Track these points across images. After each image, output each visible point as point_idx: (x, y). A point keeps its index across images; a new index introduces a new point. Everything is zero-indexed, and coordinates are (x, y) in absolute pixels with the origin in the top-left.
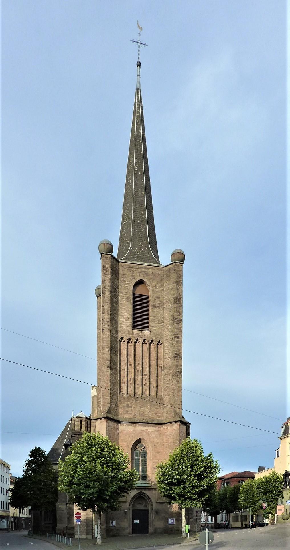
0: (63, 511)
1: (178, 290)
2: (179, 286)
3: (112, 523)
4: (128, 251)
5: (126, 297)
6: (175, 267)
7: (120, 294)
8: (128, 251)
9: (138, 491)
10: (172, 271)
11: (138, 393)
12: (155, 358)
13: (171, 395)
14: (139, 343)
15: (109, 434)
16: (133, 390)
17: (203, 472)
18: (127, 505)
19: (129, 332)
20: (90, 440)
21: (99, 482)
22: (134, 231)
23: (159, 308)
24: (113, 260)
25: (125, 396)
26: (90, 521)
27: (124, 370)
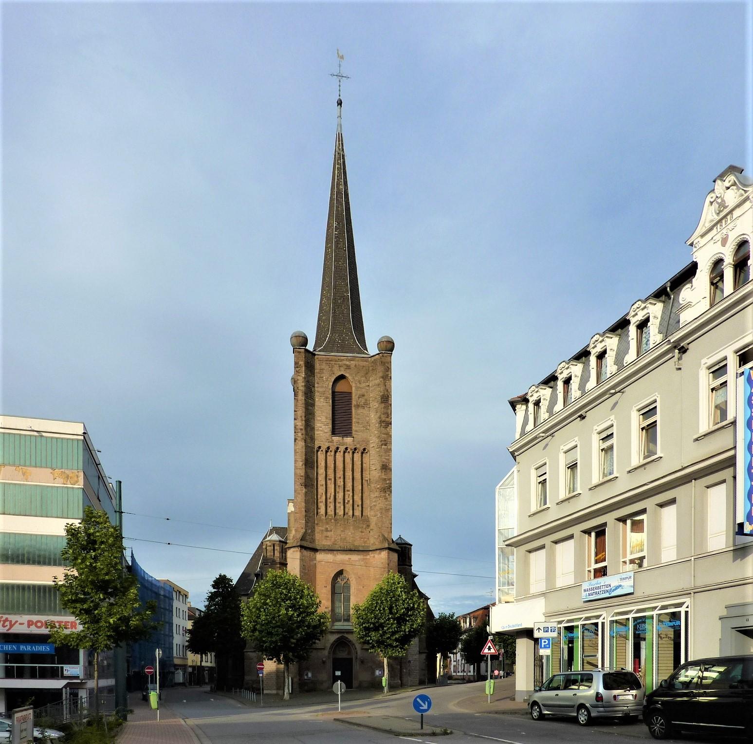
0: (252, 659)
1: (385, 386)
2: (387, 382)
3: (307, 675)
4: (327, 339)
6: (382, 358)
7: (317, 394)
8: (327, 339)
10: (378, 363)
11: (340, 514)
12: (360, 470)
14: (340, 452)
16: (333, 510)
17: (404, 614)
18: (326, 652)
20: (276, 580)
21: (283, 628)
22: (334, 313)
24: (307, 354)
25: (324, 517)
26: (281, 672)
27: (322, 485)
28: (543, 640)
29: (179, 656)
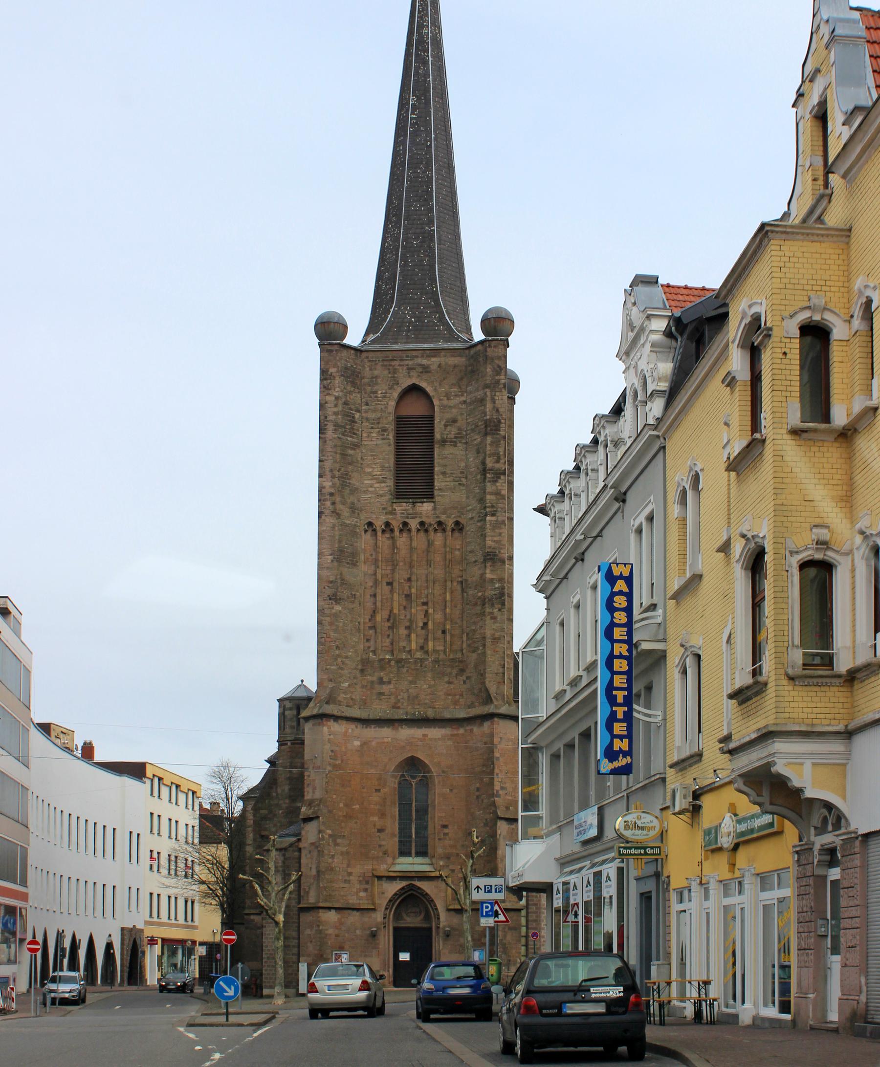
1: (494, 402)
5: (377, 430)
9: (404, 883)
13: (479, 652)
15: (332, 751)
19: (384, 509)
23: (455, 445)
28: (485, 905)
29: (173, 921)
